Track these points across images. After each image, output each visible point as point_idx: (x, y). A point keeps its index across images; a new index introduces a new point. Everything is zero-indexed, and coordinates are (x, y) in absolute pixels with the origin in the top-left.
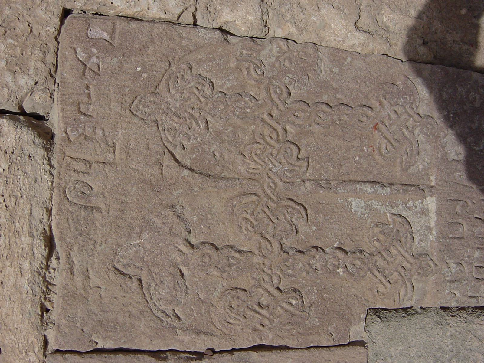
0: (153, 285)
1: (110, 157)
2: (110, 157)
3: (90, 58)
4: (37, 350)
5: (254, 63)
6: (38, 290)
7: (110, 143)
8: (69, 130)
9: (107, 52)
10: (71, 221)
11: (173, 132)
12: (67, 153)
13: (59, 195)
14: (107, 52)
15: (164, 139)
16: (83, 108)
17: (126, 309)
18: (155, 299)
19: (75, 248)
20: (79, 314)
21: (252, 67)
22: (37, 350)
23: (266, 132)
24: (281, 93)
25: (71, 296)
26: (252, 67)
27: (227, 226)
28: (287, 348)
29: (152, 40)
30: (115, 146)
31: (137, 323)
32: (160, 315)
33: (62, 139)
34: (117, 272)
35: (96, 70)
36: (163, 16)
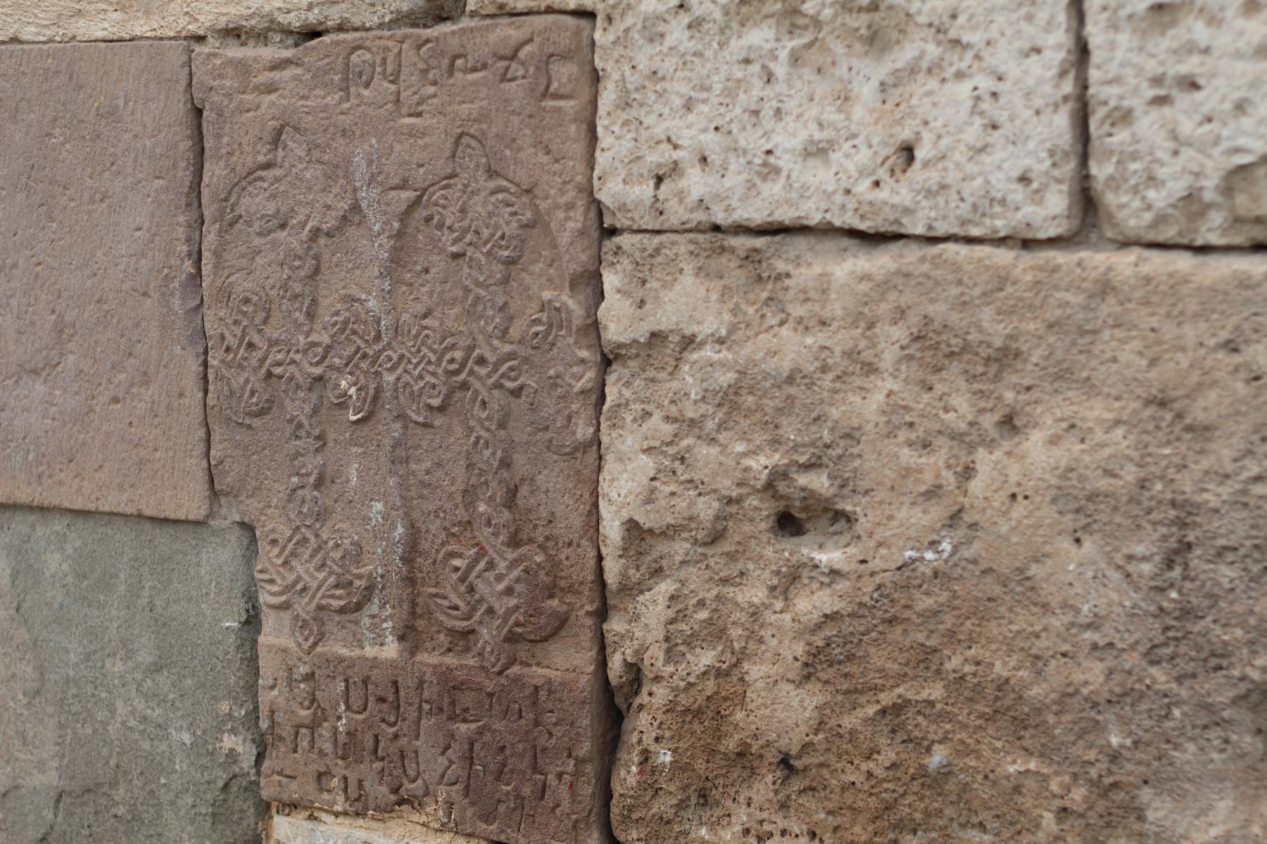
0: (266, 185)
1: (405, 110)
2: (405, 110)
3: (522, 63)
4: (190, 27)
5: (548, 332)
6: (253, 22)
7: (420, 108)
8: (430, 45)
9: (533, 90)
10: (327, 60)
11: (442, 201)
12: (405, 46)
13: (355, 40)
14: (533, 90)
15: (432, 189)
16: (459, 62)
17: (236, 147)
18: (250, 189)
19: (298, 71)
20: (227, 83)
21: (541, 328)
22: (190, 27)
23: (458, 355)
24: (510, 379)
25: (243, 69)
26: (541, 328)
27: (1148, 765)
28: (206, 392)
29: (557, 161)
30: (419, 115)
31: (222, 164)
32: (233, 199)
33: (419, 36)
34: (195, 256)
35: (509, 76)
36: (596, 174)
